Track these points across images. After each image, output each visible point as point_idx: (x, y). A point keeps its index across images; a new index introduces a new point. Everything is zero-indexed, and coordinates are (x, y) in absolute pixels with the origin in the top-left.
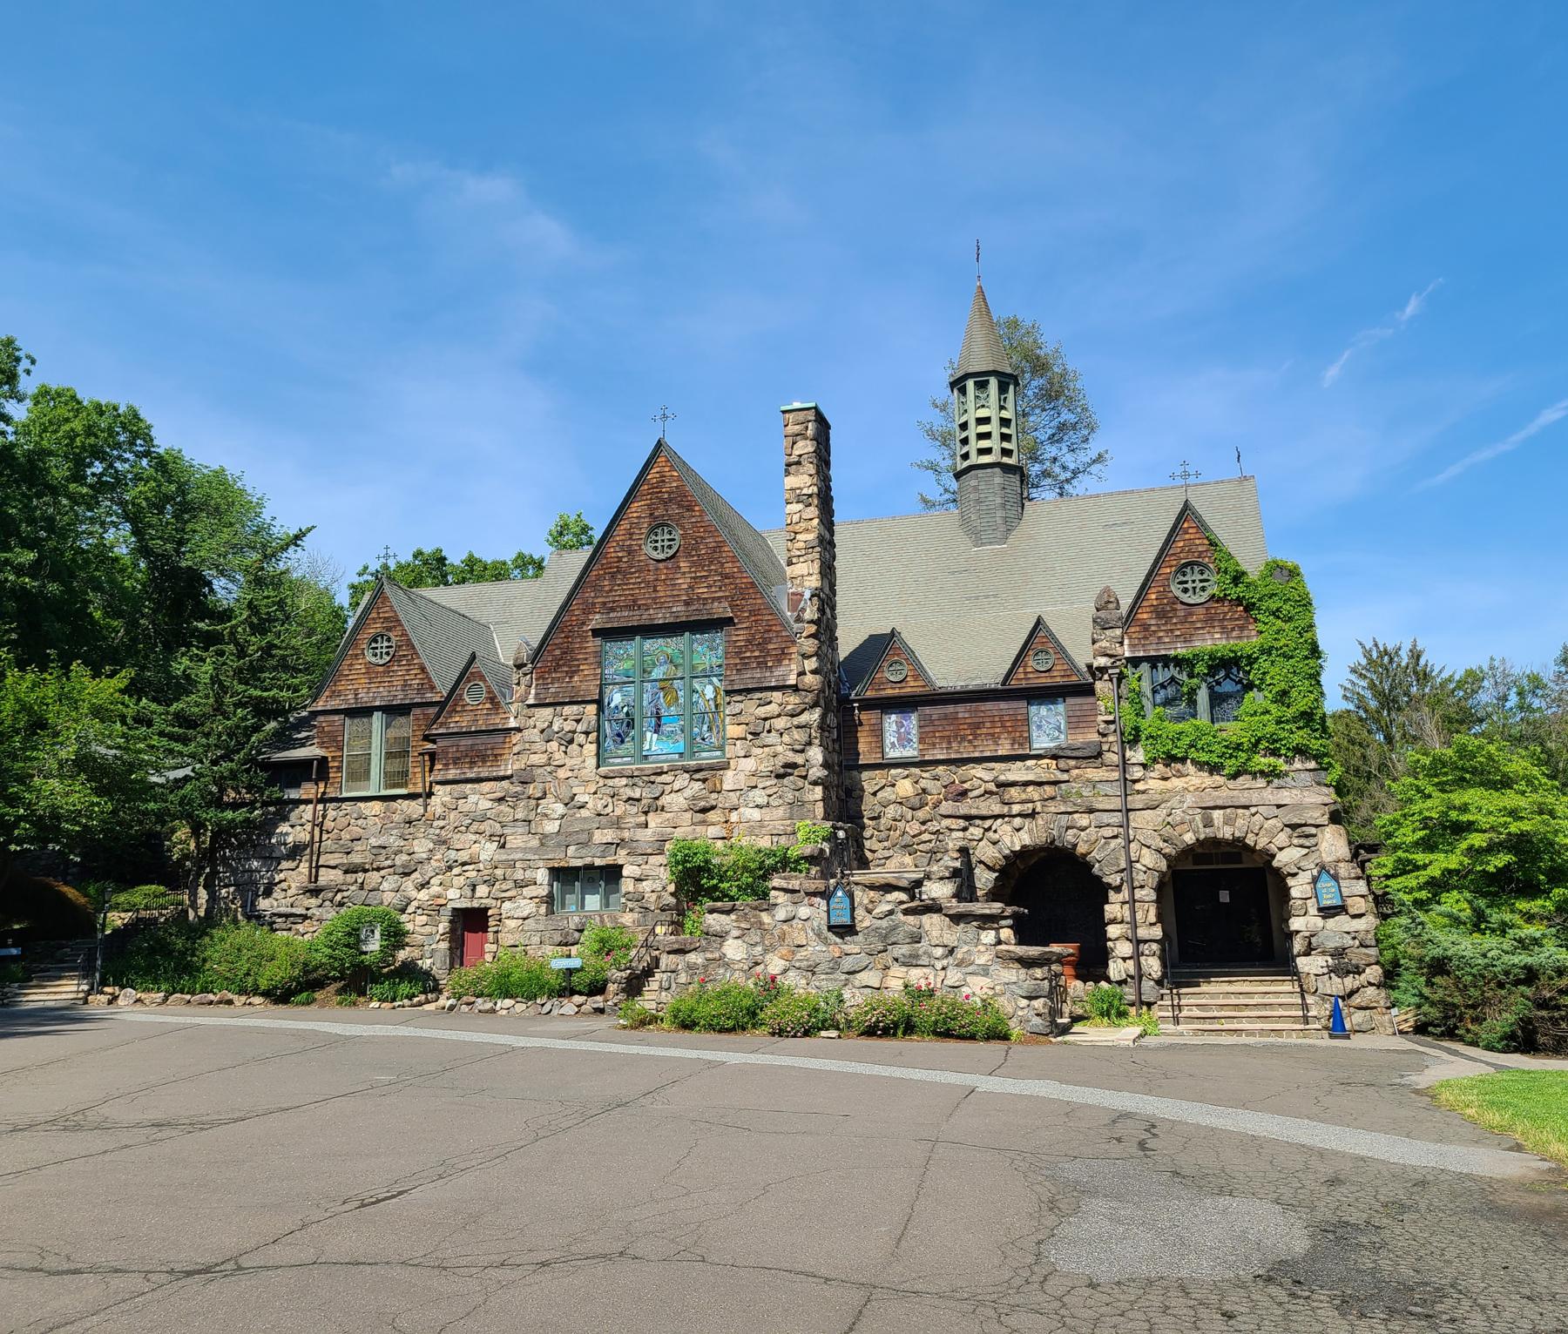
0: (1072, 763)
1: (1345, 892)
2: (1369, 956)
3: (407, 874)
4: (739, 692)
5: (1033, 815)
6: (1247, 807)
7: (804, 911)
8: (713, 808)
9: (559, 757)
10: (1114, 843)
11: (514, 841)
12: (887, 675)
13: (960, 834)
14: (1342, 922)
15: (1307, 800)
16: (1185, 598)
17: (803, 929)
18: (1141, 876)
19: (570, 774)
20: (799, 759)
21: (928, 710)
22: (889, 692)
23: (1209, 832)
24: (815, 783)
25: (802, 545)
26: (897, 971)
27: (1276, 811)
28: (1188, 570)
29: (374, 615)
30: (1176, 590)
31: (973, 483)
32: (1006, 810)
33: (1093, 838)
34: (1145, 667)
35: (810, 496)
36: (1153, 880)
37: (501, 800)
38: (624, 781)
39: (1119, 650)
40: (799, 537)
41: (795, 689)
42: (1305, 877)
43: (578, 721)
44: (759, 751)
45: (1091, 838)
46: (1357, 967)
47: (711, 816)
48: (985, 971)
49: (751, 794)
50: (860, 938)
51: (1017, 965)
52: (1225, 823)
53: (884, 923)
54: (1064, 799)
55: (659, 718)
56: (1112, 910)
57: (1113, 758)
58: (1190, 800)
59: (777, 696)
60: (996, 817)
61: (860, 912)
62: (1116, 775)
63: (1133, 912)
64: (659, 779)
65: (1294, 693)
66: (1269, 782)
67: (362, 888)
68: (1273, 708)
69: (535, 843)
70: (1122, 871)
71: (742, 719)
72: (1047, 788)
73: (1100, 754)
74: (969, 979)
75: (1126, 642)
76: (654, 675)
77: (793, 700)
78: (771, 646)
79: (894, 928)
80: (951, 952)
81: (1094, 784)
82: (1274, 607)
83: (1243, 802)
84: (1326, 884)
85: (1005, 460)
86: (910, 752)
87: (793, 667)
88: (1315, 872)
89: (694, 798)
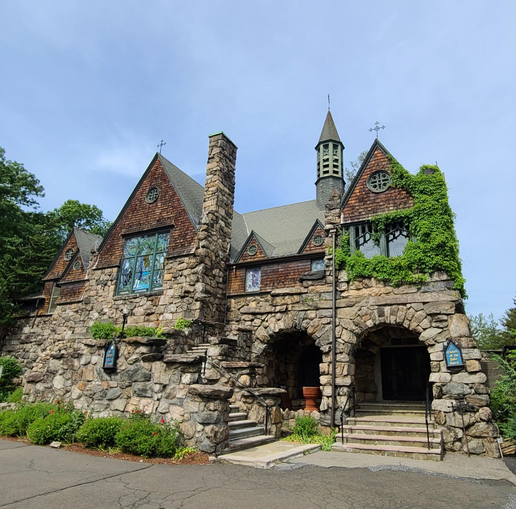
0: (310, 283)
1: (465, 356)
2: (481, 400)
3: (39, 345)
4: (171, 258)
5: (286, 311)
6: (405, 304)
7: (95, 359)
8: (153, 313)
9: (101, 291)
10: (328, 327)
11: (77, 330)
12: (248, 252)
13: (249, 323)
14: (462, 377)
15: (441, 299)
16: (374, 190)
17: (92, 370)
18: (341, 346)
19: (103, 299)
20: (191, 289)
21: (265, 268)
22: (249, 260)
23: (382, 319)
24: (197, 300)
25: (211, 193)
26: (135, 400)
27: (422, 306)
28: (377, 176)
29: (69, 242)
30: (370, 186)
31: (321, 185)
32: (273, 309)
33: (316, 324)
34: (352, 229)
35: (216, 171)
36: (346, 349)
37: (77, 312)
38: (121, 302)
39: (337, 220)
40: (209, 189)
41: (194, 255)
42: (439, 347)
43: (110, 275)
44: (176, 286)
45: (316, 324)
46: (473, 408)
47: (152, 317)
48: (181, 403)
49: (170, 306)
50: (118, 377)
51: (199, 399)
52: (391, 314)
53: (132, 367)
54: (304, 302)
55: (141, 273)
56: (323, 367)
57: (330, 279)
58: (372, 301)
59: (186, 259)
60: (268, 313)
61: (121, 361)
62: (331, 289)
63: (335, 368)
64: (135, 301)
65: (433, 235)
66: (419, 289)
67: (24, 351)
68: (422, 246)
69: (84, 331)
70: (331, 343)
71: (171, 271)
72: (295, 297)
73: (324, 277)
74: (172, 408)
75: (342, 216)
76: (142, 254)
77: (193, 260)
78: (188, 237)
79: (136, 371)
80: (165, 387)
81: (320, 294)
82: (421, 188)
83: (403, 301)
84: (452, 352)
85: (335, 175)
86: (257, 289)
87: (195, 245)
88: (446, 344)
89: (147, 309)
